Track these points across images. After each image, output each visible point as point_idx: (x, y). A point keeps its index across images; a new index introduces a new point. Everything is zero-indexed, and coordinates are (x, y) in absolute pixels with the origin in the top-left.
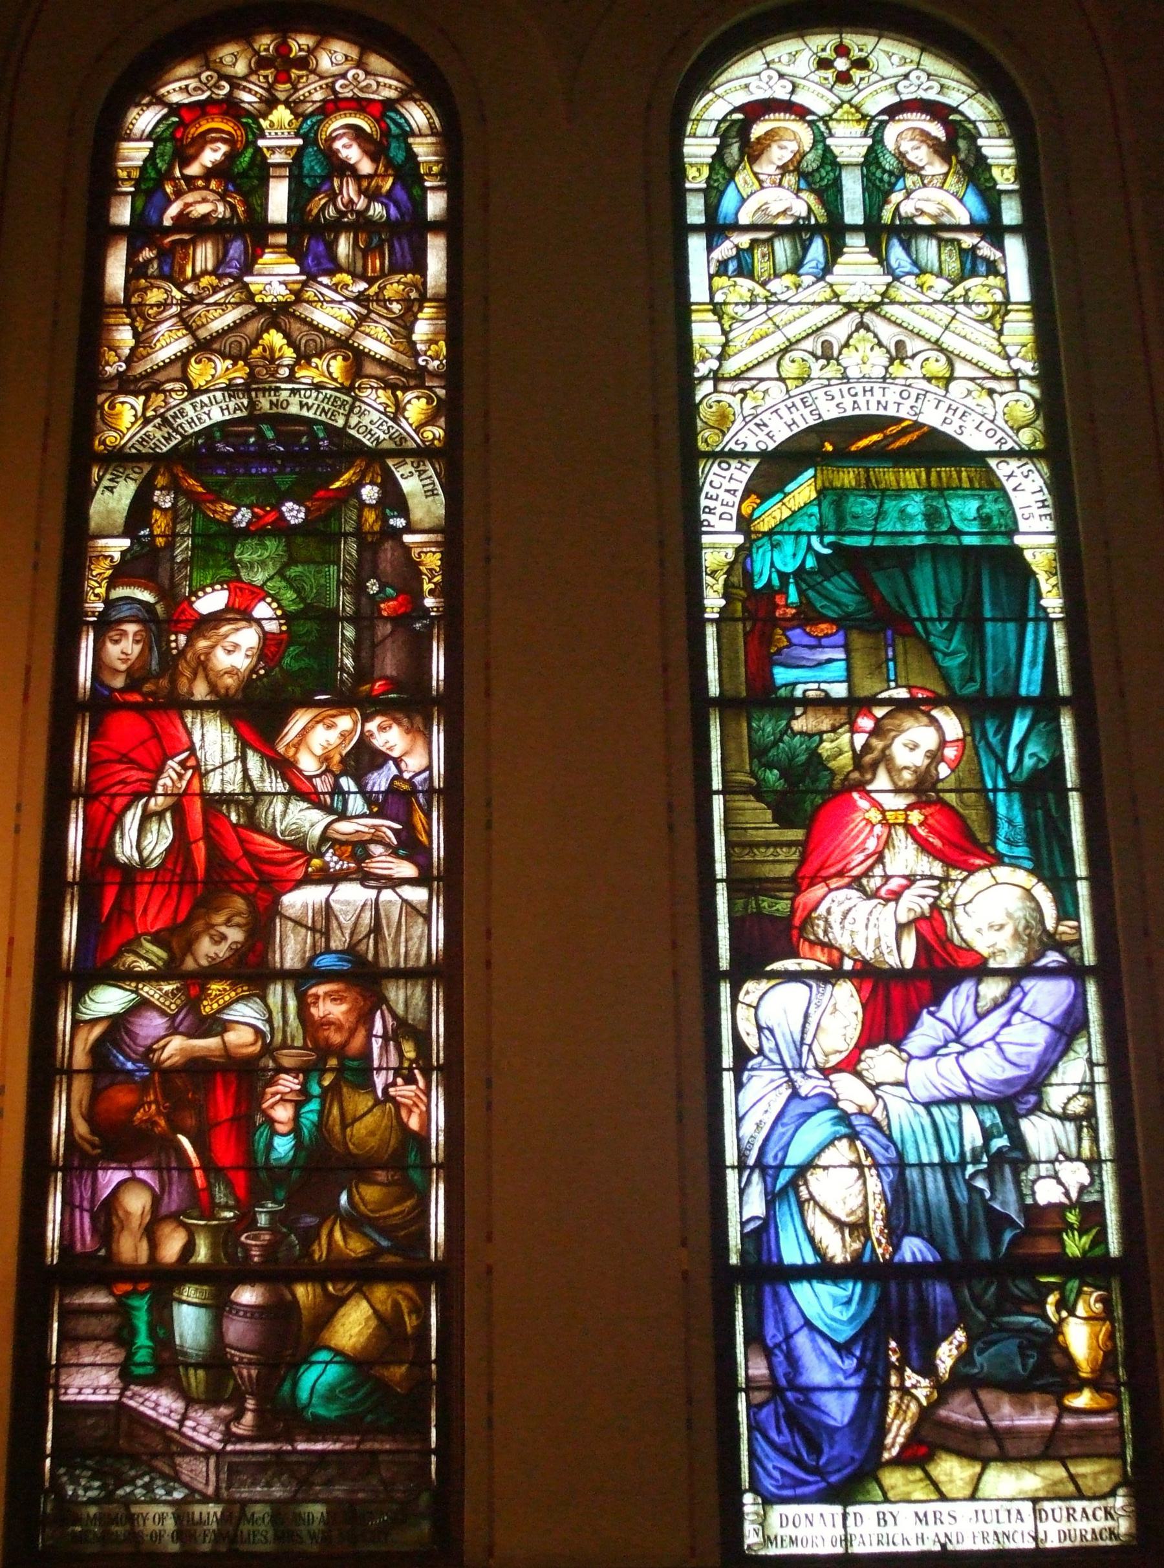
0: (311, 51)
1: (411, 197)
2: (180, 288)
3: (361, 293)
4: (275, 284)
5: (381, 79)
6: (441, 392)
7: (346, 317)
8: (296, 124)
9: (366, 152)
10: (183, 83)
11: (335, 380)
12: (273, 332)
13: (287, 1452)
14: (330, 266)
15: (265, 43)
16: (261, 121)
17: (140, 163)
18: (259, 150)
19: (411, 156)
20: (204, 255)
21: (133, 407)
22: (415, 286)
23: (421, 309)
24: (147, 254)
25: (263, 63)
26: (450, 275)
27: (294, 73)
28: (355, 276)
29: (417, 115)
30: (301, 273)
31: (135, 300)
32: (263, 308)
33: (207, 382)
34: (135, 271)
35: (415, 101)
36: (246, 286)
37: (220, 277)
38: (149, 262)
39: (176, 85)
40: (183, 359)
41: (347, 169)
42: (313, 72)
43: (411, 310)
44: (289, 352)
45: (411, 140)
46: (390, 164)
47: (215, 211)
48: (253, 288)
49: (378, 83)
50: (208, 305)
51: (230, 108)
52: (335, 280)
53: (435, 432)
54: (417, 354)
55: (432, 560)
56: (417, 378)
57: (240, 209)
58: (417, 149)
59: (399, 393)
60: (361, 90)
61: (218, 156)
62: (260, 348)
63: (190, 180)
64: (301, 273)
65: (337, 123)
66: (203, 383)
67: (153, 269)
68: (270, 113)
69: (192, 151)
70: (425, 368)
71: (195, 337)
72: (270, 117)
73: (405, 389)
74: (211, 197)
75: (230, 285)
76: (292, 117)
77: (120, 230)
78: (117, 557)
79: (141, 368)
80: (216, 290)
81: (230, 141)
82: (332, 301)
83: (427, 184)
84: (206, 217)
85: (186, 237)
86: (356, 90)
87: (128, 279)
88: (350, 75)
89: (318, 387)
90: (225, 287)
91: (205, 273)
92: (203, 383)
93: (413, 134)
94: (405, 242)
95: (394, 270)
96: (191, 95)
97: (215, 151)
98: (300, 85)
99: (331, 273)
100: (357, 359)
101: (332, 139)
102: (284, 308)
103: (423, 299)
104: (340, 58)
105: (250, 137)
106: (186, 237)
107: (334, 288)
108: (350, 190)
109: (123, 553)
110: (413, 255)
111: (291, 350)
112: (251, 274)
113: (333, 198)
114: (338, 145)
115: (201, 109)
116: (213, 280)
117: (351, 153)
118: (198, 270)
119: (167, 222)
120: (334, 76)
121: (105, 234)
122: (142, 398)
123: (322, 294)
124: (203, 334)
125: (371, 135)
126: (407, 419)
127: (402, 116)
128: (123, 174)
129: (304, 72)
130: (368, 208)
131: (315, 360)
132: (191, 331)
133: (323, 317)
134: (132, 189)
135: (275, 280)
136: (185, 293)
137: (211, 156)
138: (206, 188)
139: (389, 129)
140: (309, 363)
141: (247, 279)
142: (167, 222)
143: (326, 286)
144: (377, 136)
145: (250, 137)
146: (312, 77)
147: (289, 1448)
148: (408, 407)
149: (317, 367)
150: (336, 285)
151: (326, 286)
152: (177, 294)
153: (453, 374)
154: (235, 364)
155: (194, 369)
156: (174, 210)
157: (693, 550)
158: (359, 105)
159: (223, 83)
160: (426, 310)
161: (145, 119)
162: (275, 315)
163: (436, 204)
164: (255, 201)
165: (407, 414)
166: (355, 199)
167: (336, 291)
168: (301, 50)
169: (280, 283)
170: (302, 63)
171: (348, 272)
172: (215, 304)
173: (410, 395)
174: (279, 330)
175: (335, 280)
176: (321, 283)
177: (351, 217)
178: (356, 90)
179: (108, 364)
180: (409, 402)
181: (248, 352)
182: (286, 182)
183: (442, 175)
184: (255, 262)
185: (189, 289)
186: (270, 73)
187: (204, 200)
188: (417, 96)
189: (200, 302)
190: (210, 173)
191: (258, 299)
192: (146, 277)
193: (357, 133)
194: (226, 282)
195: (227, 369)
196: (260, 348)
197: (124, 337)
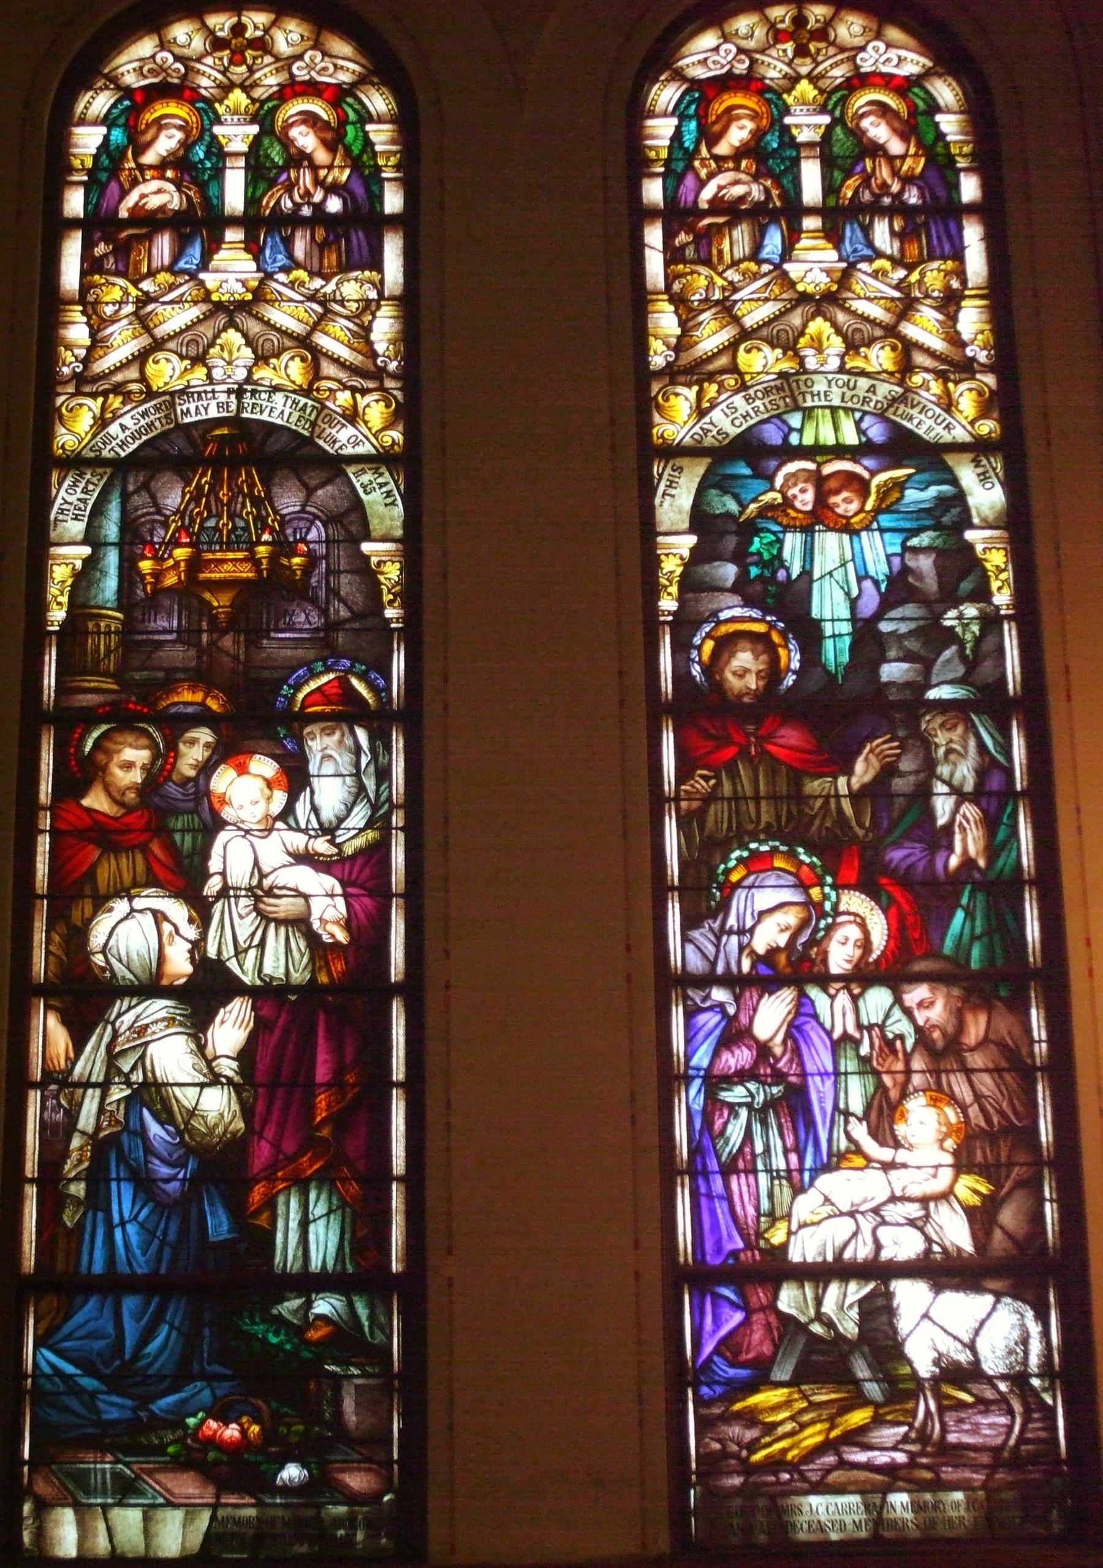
0: (829, 23)
1: (368, 190)
2: (135, 284)
3: (902, 281)
4: (816, 271)
5: (340, 62)
6: (398, 394)
7: (303, 315)
8: (821, 99)
9: (324, 143)
10: (701, 57)
11: (293, 382)
12: (231, 331)
13: (772, 1484)
14: (868, 252)
15: (221, 22)
16: (785, 96)
17: (94, 151)
18: (214, 137)
19: (368, 143)
20: (163, 246)
21: (90, 409)
22: (374, 285)
23: (379, 307)
24: (682, 238)
25: (218, 44)
26: (406, 275)
27: (249, 54)
28: (312, 274)
29: (378, 102)
30: (841, 260)
31: (676, 287)
32: (219, 306)
33: (166, 384)
34: (91, 265)
35: (373, 85)
36: (202, 283)
37: (175, 273)
38: (683, 247)
39: (695, 58)
40: (732, 347)
41: (877, 150)
42: (832, 44)
43: (368, 307)
44: (247, 352)
45: (369, 127)
46: (920, 145)
47: (749, 193)
48: (793, 276)
49: (335, 66)
50: (164, 303)
51: (750, 82)
52: (292, 277)
53: (987, 427)
54: (374, 355)
55: (392, 572)
56: (966, 368)
57: (775, 193)
58: (945, 128)
59: (951, 385)
60: (318, 73)
61: (745, 135)
62: (218, 348)
63: (718, 159)
64: (841, 260)
65: (862, 99)
66: (161, 384)
67: (110, 264)
68: (226, 97)
69: (717, 128)
70: (973, 359)
71: (152, 336)
72: (226, 102)
73: (364, 392)
74: (743, 177)
75: (770, 272)
76: (816, 92)
77: (74, 223)
78: (686, 554)
79: (686, 358)
80: (172, 287)
81: (755, 116)
82: (291, 300)
83: (384, 175)
84: (742, 199)
85: (720, 220)
86: (313, 73)
87: (84, 274)
88: (307, 57)
89: (276, 389)
90: (765, 275)
91: (163, 269)
92: (161, 384)
93: (371, 120)
94: (361, 234)
95: (931, 258)
96: (145, 77)
97: (742, 128)
98: (820, 58)
99: (869, 260)
100: (907, 348)
101: (288, 126)
102: (242, 306)
103: (82, 300)
104: (295, 37)
105: (206, 122)
106: (720, 220)
107: (291, 285)
108: (306, 178)
109: (692, 550)
110: (371, 248)
111: (249, 350)
112: (790, 260)
113: (290, 188)
114: (865, 123)
115: (726, 82)
116: (753, 266)
117: (305, 139)
118: (154, 265)
119: (123, 214)
120: (852, 49)
121: (643, 214)
122: (696, 388)
123: (280, 293)
124: (160, 332)
125: (328, 123)
126: (366, 422)
127: (361, 102)
128: (77, 163)
129: (259, 53)
130: (324, 200)
131: (273, 361)
132: (148, 330)
133: (278, 316)
134: (86, 178)
135: (231, 277)
136: (141, 290)
137: (738, 134)
138: (737, 169)
139: (347, 115)
140: (858, 353)
141: (202, 276)
142: (123, 214)
143: (283, 284)
144: (334, 123)
145: (206, 122)
146: (832, 51)
147: (773, 1479)
148: (961, 400)
149: (866, 357)
150: (292, 283)
151: (283, 284)
152: (134, 292)
153: (409, 375)
154: (784, 354)
155: (742, 357)
156: (708, 193)
157: (651, 562)
158: (312, 89)
159: (743, 57)
160: (384, 309)
161: (665, 95)
162: (231, 314)
163: (970, 189)
164: (213, 190)
165: (960, 407)
166: (889, 181)
167: (293, 289)
168: (817, 21)
169: (822, 270)
170: (821, 34)
171: (305, 269)
172: (172, 302)
173: (369, 398)
174: (237, 329)
175: (292, 277)
176: (276, 281)
177: (887, 200)
178: (313, 73)
179: (64, 364)
180: (368, 406)
181: (796, 342)
182: (242, 172)
183: (973, 155)
184: (211, 259)
185: (147, 285)
186: (789, 47)
187: (159, 191)
188: (376, 80)
189: (155, 300)
190: (739, 154)
191: (215, 297)
192: (685, 262)
193: (310, 119)
194: (766, 268)
195: (186, 369)
196: (218, 348)
197: (77, 332)
